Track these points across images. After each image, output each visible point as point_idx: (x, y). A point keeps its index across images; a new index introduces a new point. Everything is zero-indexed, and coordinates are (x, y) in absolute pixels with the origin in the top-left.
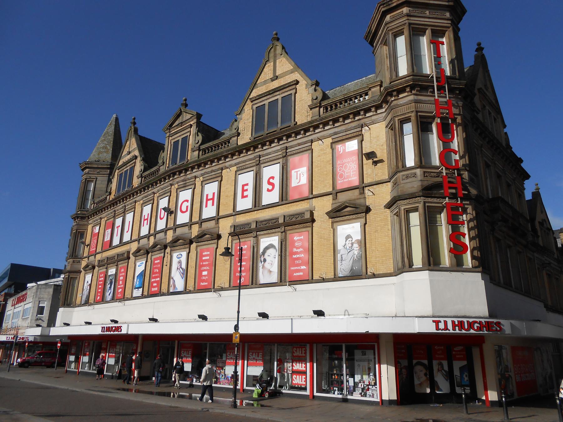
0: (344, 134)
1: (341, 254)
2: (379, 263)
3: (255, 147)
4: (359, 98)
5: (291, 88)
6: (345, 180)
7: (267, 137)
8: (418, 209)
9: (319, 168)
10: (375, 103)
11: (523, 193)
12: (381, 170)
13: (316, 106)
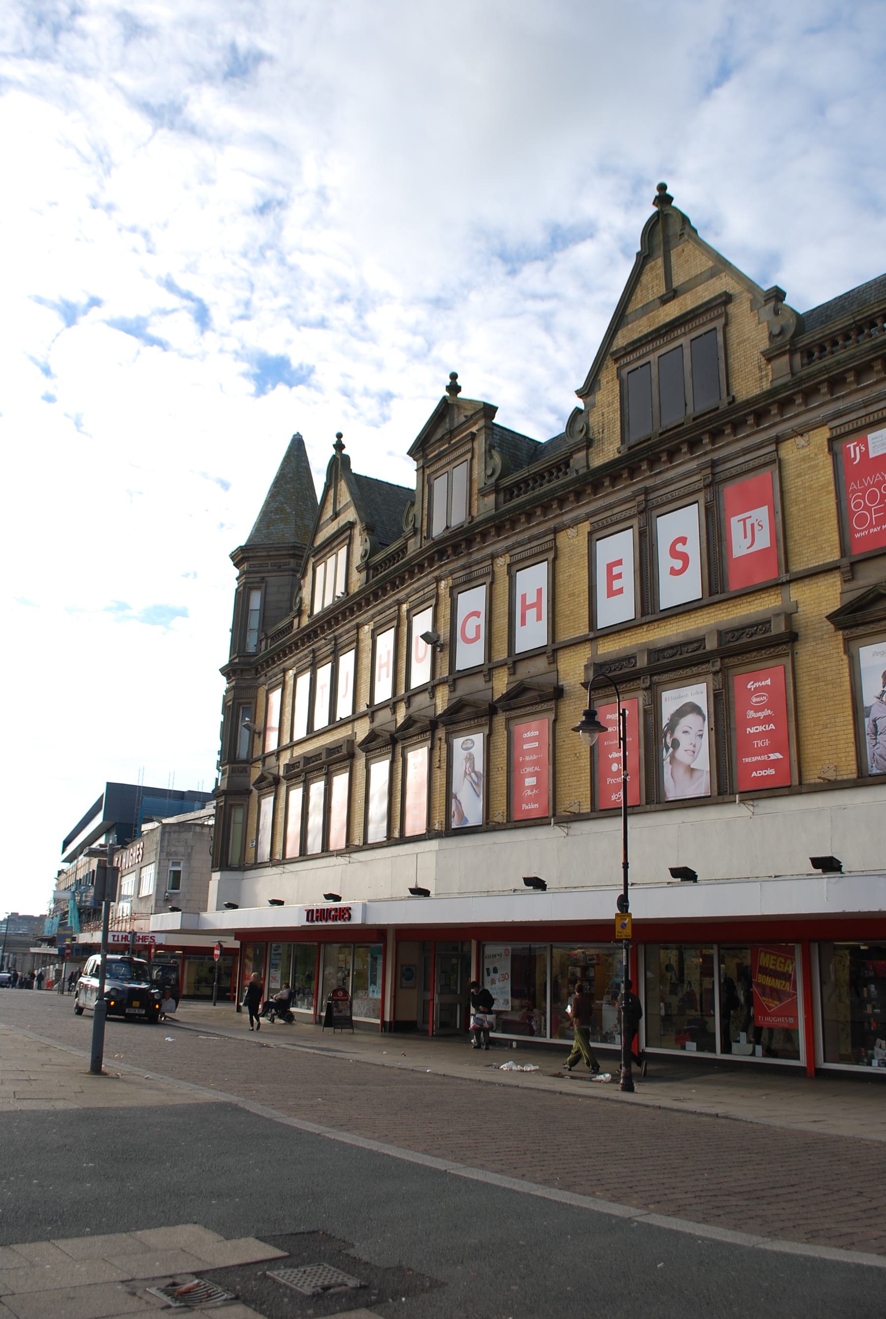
0: (862, 412)
1: (872, 717)
7: (662, 442)
9: (802, 506)
13: (783, 350)
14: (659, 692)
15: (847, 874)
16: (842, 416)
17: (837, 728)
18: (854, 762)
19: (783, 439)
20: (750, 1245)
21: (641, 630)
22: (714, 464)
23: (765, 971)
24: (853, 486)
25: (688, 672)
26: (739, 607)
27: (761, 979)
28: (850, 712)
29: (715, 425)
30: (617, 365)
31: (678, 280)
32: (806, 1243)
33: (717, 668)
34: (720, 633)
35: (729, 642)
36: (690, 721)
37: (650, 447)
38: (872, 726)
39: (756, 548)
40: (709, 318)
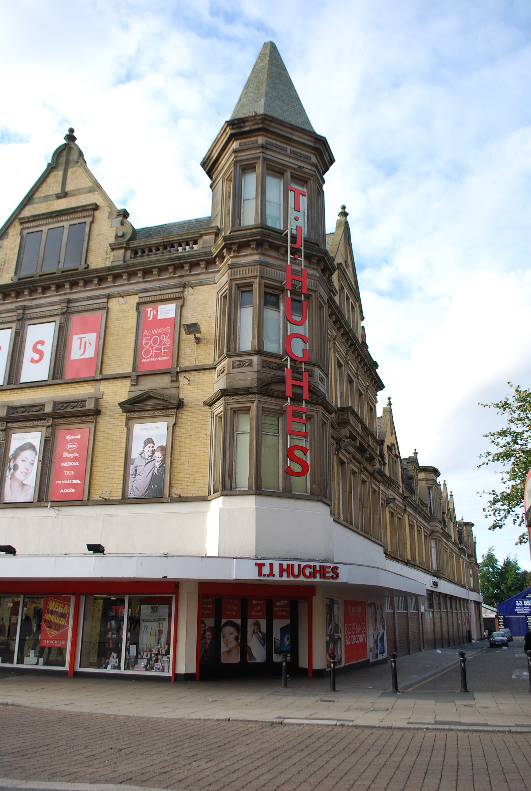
0: (158, 293)
1: (135, 465)
2: (189, 481)
3: (19, 294)
4: (183, 246)
5: (86, 214)
6: (152, 359)
7: (40, 281)
8: (249, 410)
9: (116, 337)
10: (207, 256)
11: (375, 406)
12: (204, 352)
13: (121, 246)
14: (10, 433)
15: (107, 555)
16: (146, 292)
17: (115, 469)
18: (121, 490)
19: (112, 297)
20: (12, 787)
21: (6, 393)
22: (69, 301)
23: (52, 613)
24: (146, 332)
25: (31, 424)
26: (69, 389)
27: (48, 617)
28: (123, 460)
29: (74, 278)
30: (22, 227)
31: (68, 188)
32: (48, 781)
33: (50, 424)
34: (55, 403)
35: (60, 409)
36: (28, 454)
37: (32, 282)
38: (134, 470)
39: (86, 356)
40: (83, 215)
